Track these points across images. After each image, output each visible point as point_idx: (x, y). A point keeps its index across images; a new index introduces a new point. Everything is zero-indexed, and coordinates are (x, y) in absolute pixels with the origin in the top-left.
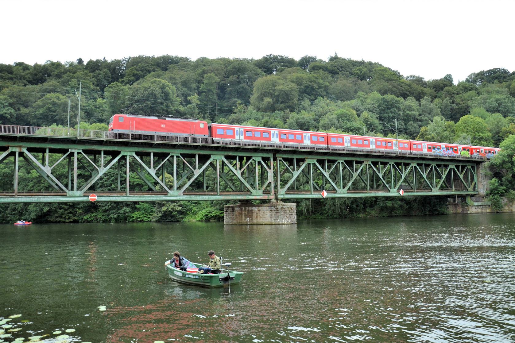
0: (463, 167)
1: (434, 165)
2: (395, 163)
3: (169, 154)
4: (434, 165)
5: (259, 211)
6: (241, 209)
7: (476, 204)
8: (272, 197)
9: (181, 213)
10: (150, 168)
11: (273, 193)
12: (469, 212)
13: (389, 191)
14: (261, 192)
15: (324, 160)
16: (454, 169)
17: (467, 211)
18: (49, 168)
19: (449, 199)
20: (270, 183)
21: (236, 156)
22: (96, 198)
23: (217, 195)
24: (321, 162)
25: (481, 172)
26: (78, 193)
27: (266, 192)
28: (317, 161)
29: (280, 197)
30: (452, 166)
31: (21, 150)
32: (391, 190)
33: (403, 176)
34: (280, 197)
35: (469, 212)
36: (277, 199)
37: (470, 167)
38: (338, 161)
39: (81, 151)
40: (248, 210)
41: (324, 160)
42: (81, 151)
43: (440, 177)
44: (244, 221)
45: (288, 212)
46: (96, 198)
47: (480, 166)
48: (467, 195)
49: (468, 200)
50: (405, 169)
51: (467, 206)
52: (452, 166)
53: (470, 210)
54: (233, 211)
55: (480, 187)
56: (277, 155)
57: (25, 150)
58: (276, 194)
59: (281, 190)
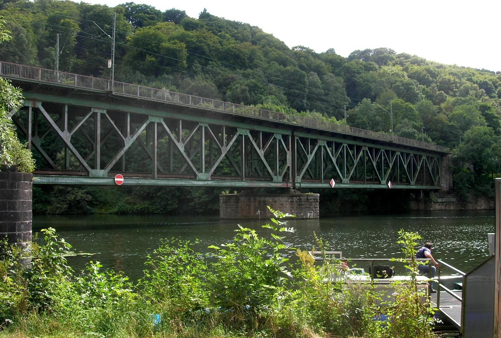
0: (267, 136)
1: (345, 145)
2: (109, 112)
3: (197, 123)
4: (345, 145)
5: (275, 202)
6: (249, 200)
7: (440, 200)
8: (290, 185)
9: (90, 203)
10: (63, 130)
11: (291, 181)
12: (432, 209)
13: (380, 183)
14: (208, 175)
15: (124, 114)
16: (247, 138)
17: (431, 208)
18: (68, 134)
19: (411, 194)
20: (289, 167)
21: (260, 132)
22: (122, 180)
23: (242, 181)
24: (173, 124)
25: (445, 165)
26: (101, 173)
27: (285, 178)
28: (164, 121)
29: (297, 185)
30: (322, 143)
31: (34, 104)
32: (93, 172)
33: (225, 151)
34: (297, 185)
35: (432, 209)
36: (294, 188)
37: (279, 137)
38: (200, 124)
39: (105, 112)
40: (260, 202)
41: (258, 132)
42: (105, 112)
43: (388, 167)
44: (252, 214)
45: (314, 204)
46: (122, 180)
47: (444, 158)
48: (431, 190)
49: (433, 196)
50: (229, 139)
51: (431, 203)
52: (244, 131)
53: (433, 206)
54: (237, 202)
55: (443, 182)
56: (295, 134)
57: (40, 106)
58: (294, 181)
59: (298, 177)
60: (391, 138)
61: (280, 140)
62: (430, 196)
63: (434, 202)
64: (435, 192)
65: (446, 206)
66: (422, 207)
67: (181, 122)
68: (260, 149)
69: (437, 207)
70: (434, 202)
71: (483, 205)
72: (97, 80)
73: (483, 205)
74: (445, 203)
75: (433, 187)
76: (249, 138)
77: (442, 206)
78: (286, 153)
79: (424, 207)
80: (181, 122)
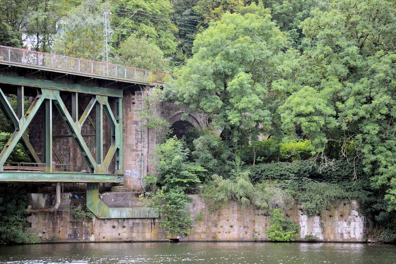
0: (84, 100)
7: (114, 213)
17: (87, 234)
35: (92, 238)
37: (104, 101)
48: (92, 185)
49: (94, 200)
53: (97, 231)
55: (131, 162)
60: (53, 93)
61: (105, 106)
62: (88, 197)
63: (97, 218)
64: (101, 192)
65: (132, 232)
66: (64, 231)
67: (23, 88)
68: (75, 121)
69: (107, 232)
70: (97, 218)
71: (236, 227)
72: (14, 50)
73: (236, 227)
74: (131, 221)
75: (91, 177)
76: (58, 105)
77: (120, 230)
78: (114, 126)
79: (70, 232)
80: (23, 88)
